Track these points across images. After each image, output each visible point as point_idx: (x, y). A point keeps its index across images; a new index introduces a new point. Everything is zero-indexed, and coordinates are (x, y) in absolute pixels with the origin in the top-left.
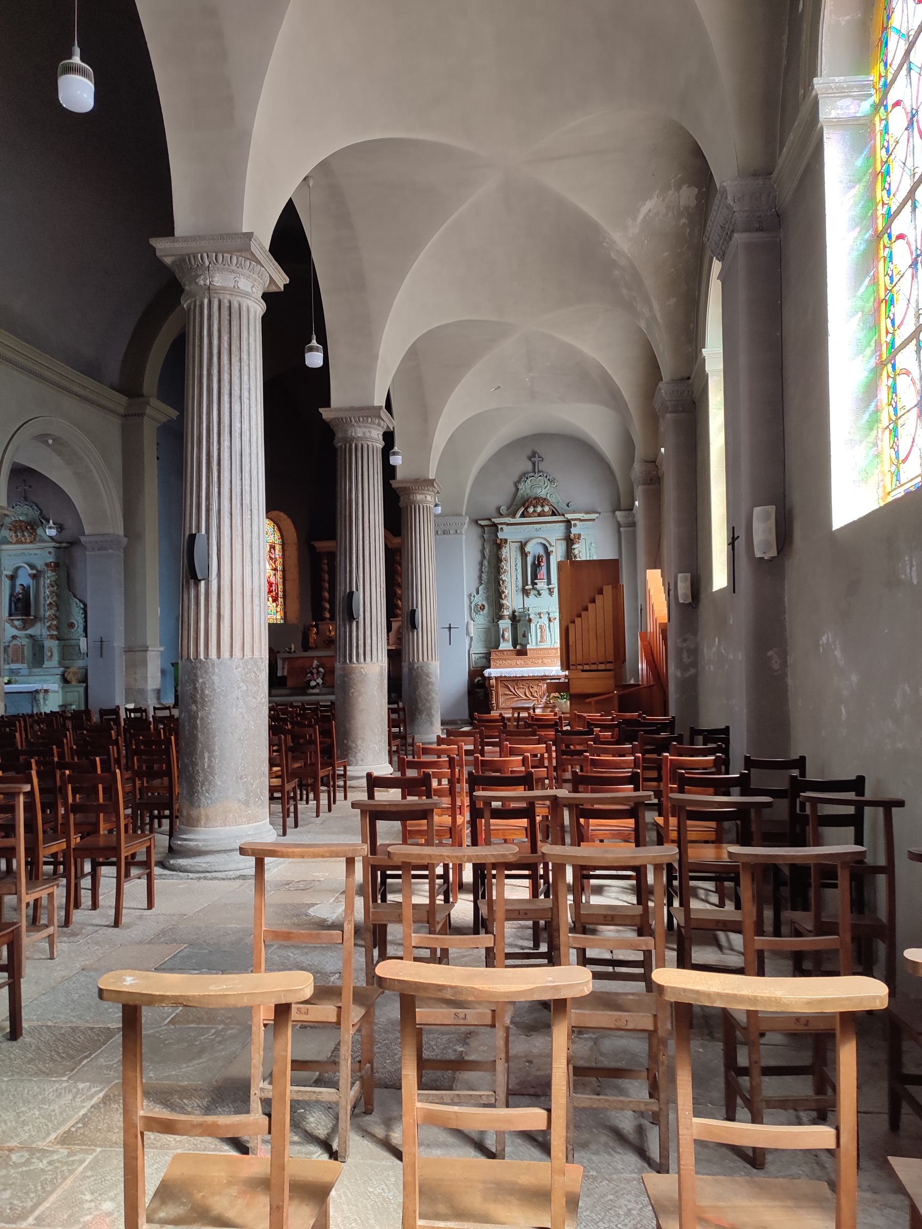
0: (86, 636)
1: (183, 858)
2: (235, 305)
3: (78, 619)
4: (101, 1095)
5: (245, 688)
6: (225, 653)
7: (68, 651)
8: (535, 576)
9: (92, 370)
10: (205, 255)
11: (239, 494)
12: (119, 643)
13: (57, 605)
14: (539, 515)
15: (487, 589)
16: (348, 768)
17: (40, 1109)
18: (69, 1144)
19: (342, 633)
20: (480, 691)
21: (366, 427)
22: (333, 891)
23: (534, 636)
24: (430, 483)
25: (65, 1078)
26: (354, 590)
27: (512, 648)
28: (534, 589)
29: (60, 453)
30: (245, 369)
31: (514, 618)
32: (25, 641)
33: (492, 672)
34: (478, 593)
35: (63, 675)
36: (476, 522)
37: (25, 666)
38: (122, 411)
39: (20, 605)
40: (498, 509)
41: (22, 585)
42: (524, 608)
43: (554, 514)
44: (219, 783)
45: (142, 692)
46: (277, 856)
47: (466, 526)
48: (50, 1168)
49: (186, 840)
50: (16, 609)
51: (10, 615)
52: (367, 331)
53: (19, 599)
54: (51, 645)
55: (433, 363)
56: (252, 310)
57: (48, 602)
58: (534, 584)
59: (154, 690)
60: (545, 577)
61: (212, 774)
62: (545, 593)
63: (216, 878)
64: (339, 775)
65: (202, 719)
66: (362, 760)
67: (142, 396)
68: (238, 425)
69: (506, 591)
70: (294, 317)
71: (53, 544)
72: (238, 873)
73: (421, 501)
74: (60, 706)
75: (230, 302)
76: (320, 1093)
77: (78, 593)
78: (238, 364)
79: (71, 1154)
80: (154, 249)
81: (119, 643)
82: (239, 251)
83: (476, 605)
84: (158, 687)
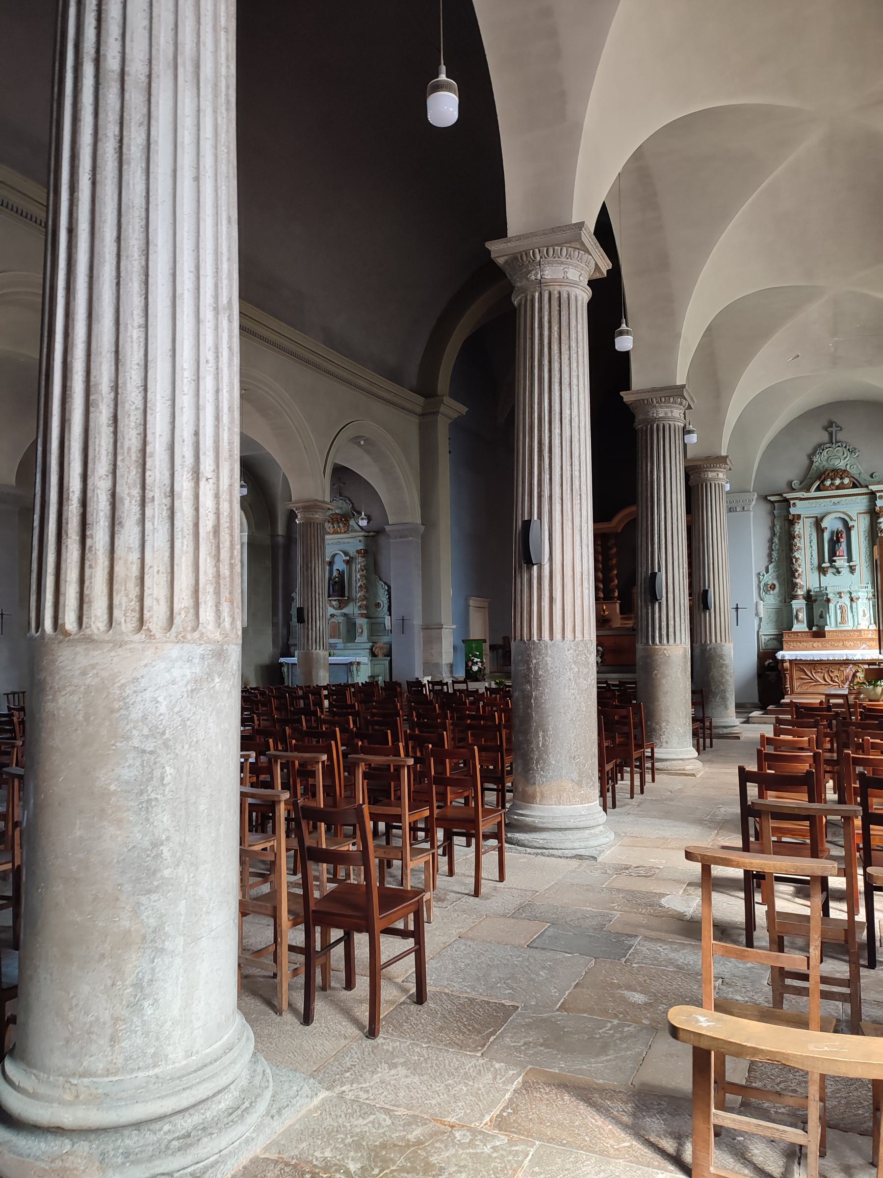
0: (390, 615)
1: (520, 832)
2: (564, 296)
3: (383, 599)
4: (520, 1079)
5: (576, 670)
6: (558, 635)
7: (375, 629)
8: (833, 553)
9: (394, 375)
10: (537, 250)
11: (569, 479)
12: (417, 621)
13: (366, 588)
14: (838, 488)
15: (778, 567)
16: (656, 750)
17: (466, 1085)
18: (506, 1131)
19: (644, 614)
20: (772, 675)
21: (668, 407)
22: (678, 881)
23: (833, 617)
24: (723, 460)
25: (479, 1054)
26: (657, 571)
27: (807, 630)
28: (832, 566)
29: (368, 452)
30: (574, 356)
31: (809, 597)
32: (341, 619)
33: (786, 654)
34: (767, 572)
35: (371, 649)
36: (765, 498)
37: (341, 640)
38: (419, 410)
39: (336, 587)
40: (790, 484)
42: (820, 587)
43: (855, 486)
44: (554, 762)
45: (437, 666)
46: (732, 866)
47: (754, 502)
48: (495, 1155)
49: (522, 815)
51: (329, 597)
52: (668, 310)
54: (362, 622)
55: (736, 334)
56: (579, 298)
58: (832, 561)
59: (448, 664)
60: (845, 554)
61: (546, 752)
62: (845, 571)
63: (553, 856)
64: (648, 757)
65: (536, 698)
66: (667, 742)
67: (437, 396)
68: (568, 412)
69: (800, 570)
70: (607, 304)
71: (363, 533)
72: (575, 852)
73: (714, 479)
74: (369, 677)
75: (559, 293)
76: (785, 1132)
77: (383, 576)
78: (567, 352)
79: (511, 1142)
80: (489, 252)
81: (417, 621)
82: (570, 242)
83: (766, 585)
84: (451, 661)
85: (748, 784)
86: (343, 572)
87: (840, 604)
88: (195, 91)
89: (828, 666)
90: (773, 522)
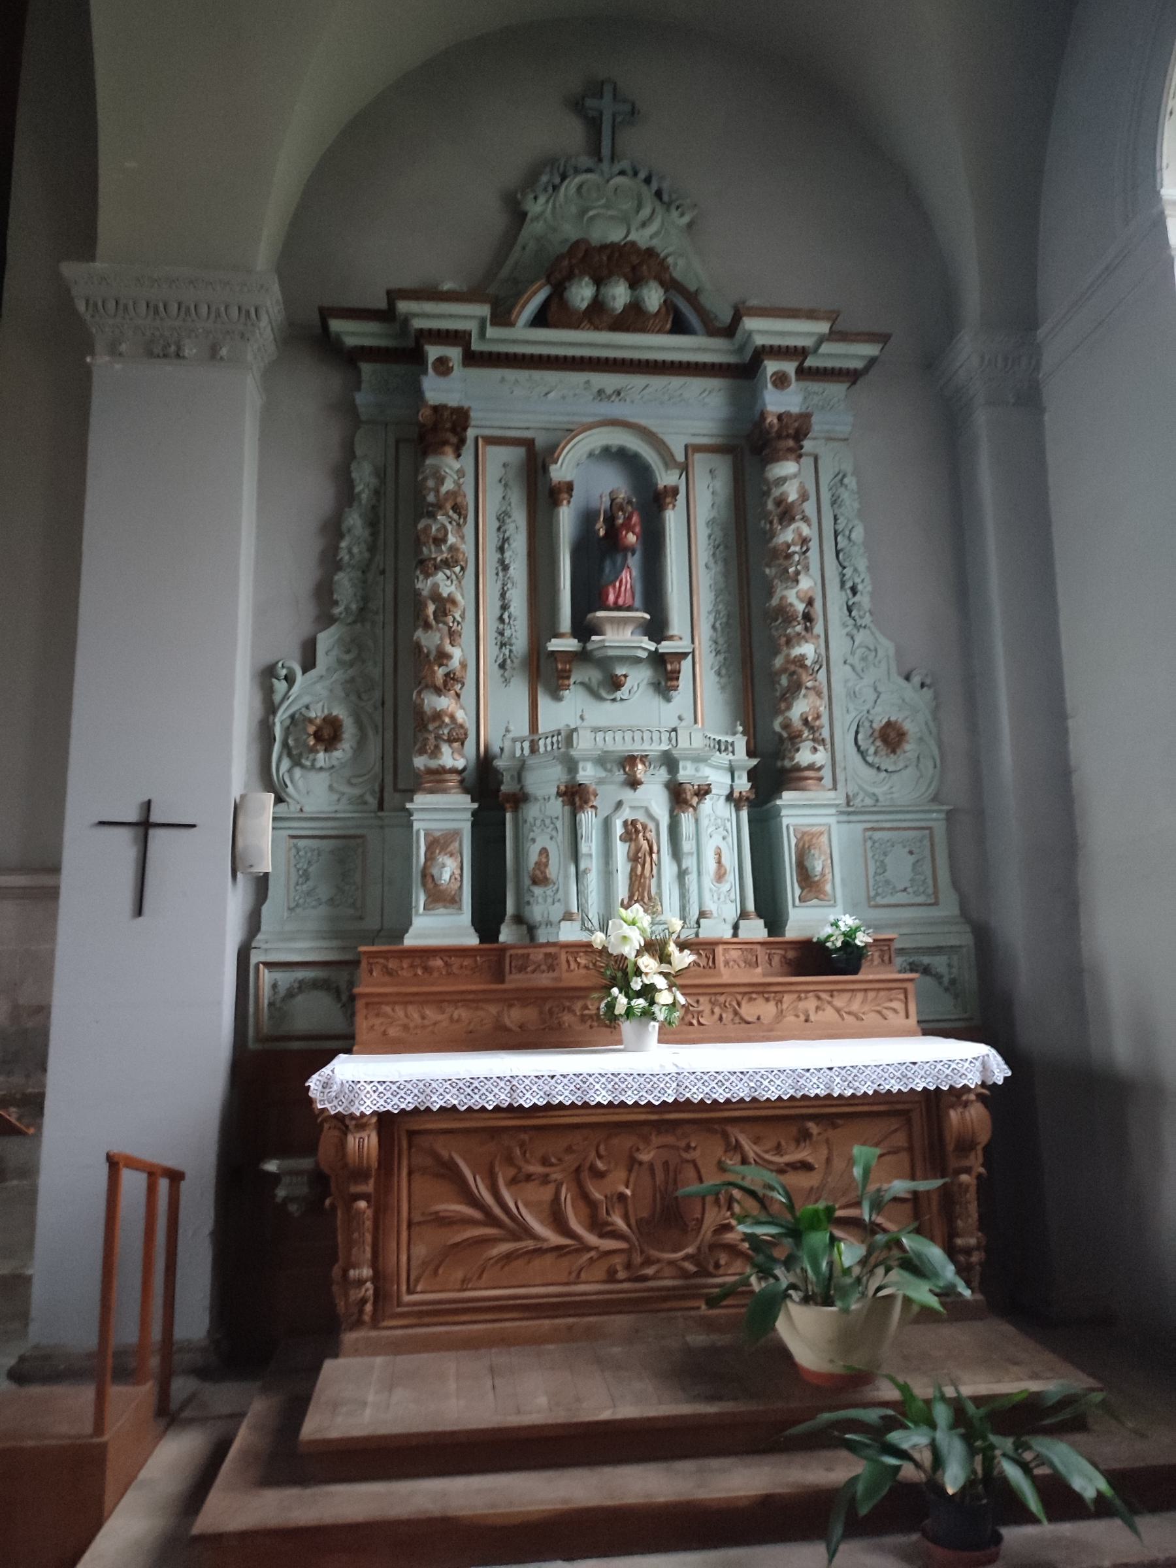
8: (590, 596)
15: (356, 650)
27: (473, 940)
31: (493, 793)
34: (309, 664)
43: (680, 327)
58: (583, 629)
87: (627, 814)
88: (240, 843)
90: (350, 453)
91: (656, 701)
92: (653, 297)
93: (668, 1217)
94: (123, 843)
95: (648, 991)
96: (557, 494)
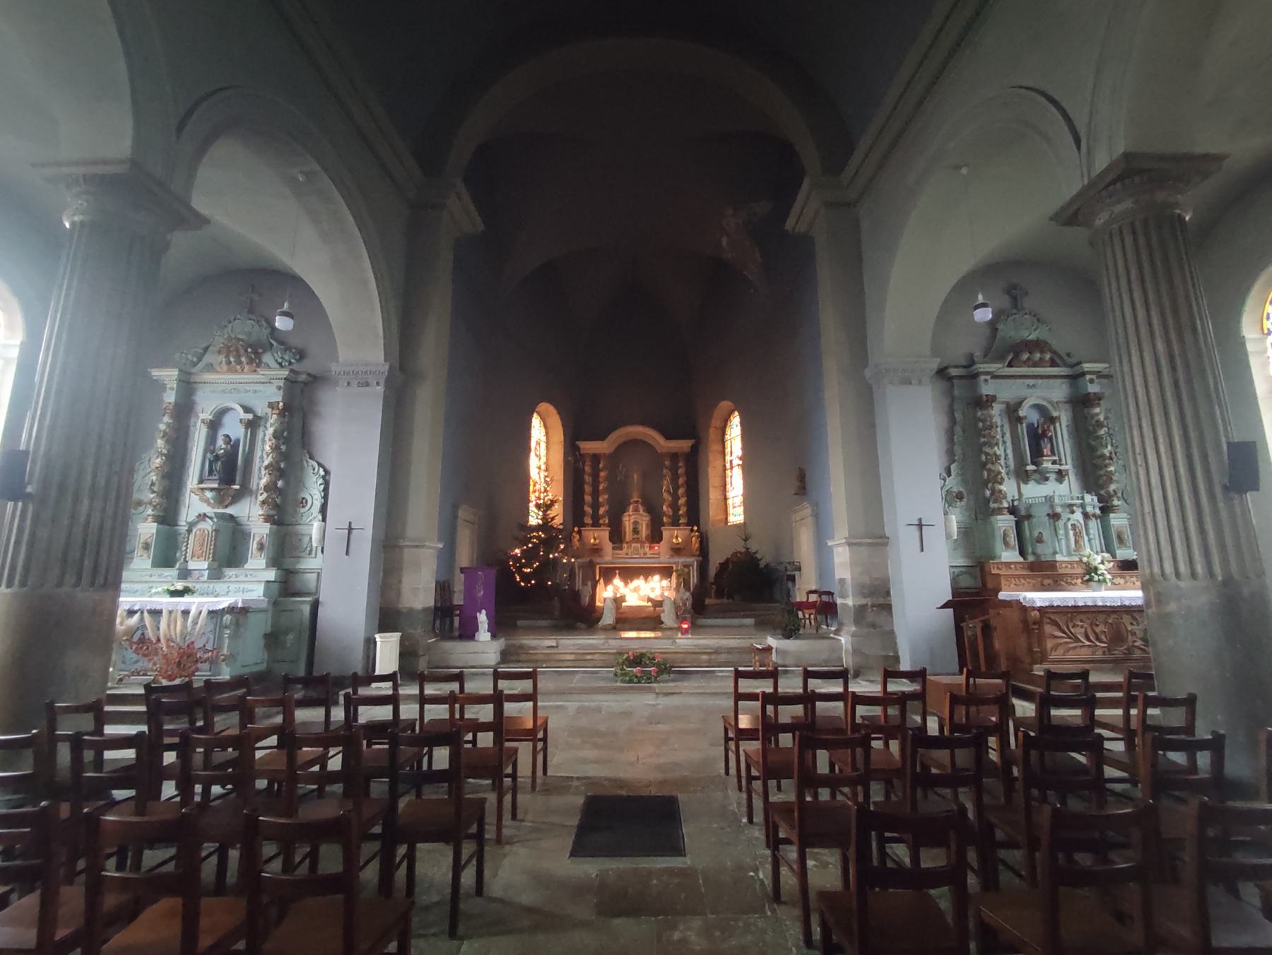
0: (324, 520)
3: (313, 492)
14: (1035, 365)
34: (949, 475)
41: (227, 436)
43: (1053, 364)
50: (211, 472)
51: (201, 481)
53: (217, 458)
57: (266, 463)
59: (672, 556)
85: (491, 733)
86: (238, 441)
89: (1090, 616)
91: (1057, 484)
92: (1048, 356)
93: (1117, 637)
94: (915, 531)
95: (1102, 574)
96: (1020, 420)
